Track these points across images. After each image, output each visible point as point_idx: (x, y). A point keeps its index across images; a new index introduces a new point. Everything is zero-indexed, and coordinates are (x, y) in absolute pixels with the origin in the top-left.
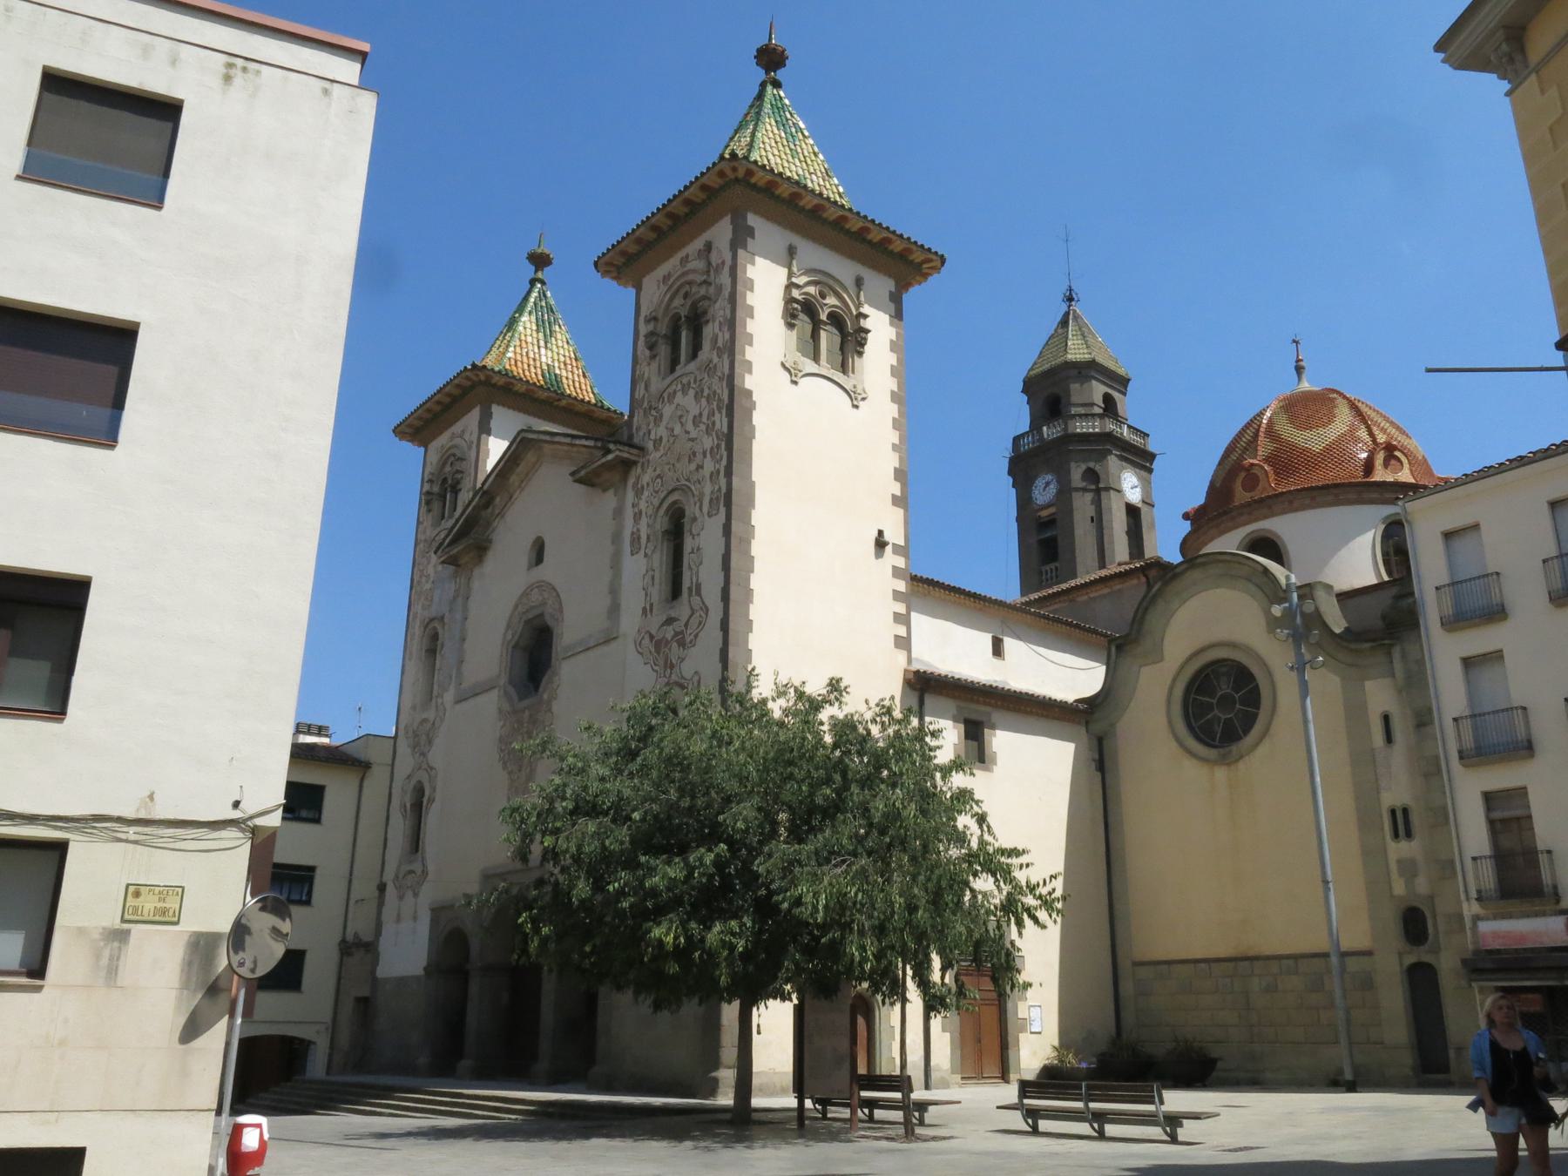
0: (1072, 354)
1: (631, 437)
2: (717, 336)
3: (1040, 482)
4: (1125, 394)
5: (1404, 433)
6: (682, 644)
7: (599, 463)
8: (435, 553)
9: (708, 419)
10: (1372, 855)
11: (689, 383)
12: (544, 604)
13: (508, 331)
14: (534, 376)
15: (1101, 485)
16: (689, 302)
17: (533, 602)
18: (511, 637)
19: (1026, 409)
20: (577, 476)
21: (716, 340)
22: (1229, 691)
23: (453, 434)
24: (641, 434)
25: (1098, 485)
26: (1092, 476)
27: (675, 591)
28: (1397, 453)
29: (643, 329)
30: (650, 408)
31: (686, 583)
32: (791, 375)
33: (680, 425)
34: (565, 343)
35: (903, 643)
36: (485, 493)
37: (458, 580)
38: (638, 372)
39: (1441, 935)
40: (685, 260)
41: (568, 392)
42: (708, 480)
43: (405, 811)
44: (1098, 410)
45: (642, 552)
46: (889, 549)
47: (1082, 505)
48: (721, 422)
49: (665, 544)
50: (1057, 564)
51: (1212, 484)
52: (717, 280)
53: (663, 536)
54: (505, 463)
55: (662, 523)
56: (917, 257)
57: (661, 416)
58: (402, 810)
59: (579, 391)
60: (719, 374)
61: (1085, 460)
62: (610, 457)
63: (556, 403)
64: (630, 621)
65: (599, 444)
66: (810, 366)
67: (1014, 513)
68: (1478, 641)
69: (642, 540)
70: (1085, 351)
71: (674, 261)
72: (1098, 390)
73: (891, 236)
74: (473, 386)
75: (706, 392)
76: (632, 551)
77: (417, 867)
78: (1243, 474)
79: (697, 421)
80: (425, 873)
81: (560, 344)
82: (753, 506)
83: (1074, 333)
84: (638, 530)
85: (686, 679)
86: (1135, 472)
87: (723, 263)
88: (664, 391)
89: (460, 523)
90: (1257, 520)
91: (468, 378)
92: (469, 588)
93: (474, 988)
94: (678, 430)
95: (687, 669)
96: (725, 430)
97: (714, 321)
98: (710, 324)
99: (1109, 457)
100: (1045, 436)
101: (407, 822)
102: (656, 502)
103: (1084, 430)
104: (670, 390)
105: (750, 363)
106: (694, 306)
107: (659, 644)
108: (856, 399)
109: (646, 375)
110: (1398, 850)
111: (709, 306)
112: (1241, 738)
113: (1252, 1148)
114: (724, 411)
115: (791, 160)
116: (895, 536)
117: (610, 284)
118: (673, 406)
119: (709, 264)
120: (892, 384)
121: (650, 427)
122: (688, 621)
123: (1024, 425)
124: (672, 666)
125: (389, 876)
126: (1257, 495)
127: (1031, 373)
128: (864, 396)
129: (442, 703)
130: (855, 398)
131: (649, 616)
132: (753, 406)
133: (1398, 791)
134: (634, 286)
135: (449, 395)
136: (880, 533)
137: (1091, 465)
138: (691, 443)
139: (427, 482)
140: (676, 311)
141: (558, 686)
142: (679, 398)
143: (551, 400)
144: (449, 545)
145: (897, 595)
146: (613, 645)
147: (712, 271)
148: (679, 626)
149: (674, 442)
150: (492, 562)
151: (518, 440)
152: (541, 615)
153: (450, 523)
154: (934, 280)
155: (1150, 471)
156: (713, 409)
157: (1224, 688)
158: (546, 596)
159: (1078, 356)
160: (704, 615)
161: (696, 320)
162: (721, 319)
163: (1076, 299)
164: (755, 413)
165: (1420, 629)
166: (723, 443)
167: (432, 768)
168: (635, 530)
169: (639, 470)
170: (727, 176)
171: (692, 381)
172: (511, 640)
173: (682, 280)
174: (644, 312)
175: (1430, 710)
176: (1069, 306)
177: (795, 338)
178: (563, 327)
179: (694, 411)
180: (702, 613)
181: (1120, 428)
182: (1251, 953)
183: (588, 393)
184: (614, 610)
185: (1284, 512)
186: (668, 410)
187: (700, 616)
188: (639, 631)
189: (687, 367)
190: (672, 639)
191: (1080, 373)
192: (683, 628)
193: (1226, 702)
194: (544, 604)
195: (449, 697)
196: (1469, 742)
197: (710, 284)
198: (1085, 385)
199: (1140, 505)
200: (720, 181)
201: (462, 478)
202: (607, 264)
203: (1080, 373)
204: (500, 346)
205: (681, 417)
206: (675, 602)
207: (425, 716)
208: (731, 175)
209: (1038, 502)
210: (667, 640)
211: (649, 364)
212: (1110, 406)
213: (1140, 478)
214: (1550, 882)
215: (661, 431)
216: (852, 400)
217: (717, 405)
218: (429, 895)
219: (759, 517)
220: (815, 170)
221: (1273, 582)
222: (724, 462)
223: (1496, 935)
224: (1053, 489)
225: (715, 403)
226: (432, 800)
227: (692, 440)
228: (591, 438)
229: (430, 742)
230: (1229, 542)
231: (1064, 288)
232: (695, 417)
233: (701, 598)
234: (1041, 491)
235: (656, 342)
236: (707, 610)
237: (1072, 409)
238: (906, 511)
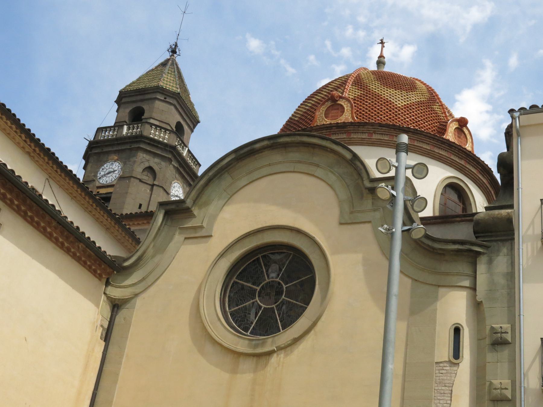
22: (278, 280)
163: (178, 53)
181: (183, 148)
212: (179, 130)
231: (172, 42)
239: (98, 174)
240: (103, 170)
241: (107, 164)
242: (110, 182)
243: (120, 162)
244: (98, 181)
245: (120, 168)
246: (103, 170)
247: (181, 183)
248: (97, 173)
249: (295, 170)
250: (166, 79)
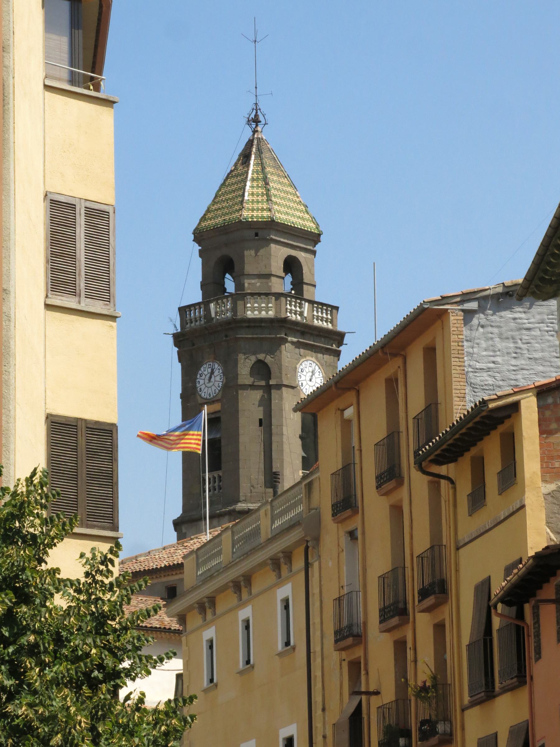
0: (249, 210)
3: (205, 370)
15: (272, 382)
19: (198, 262)
61: (254, 353)
67: (179, 391)
83: (255, 176)
86: (317, 358)
99: (283, 347)
100: (213, 315)
127: (203, 224)
137: (261, 356)
159: (255, 214)
176: (255, 131)
191: (257, 235)
198: (262, 252)
203: (257, 235)
209: (203, 395)
224: (218, 380)
234: (207, 381)
239: (197, 384)
240: (201, 376)
241: (204, 366)
242: (214, 395)
243: (218, 362)
244: (199, 394)
245: (221, 371)
246: (201, 376)
247: (312, 357)
248: (196, 383)
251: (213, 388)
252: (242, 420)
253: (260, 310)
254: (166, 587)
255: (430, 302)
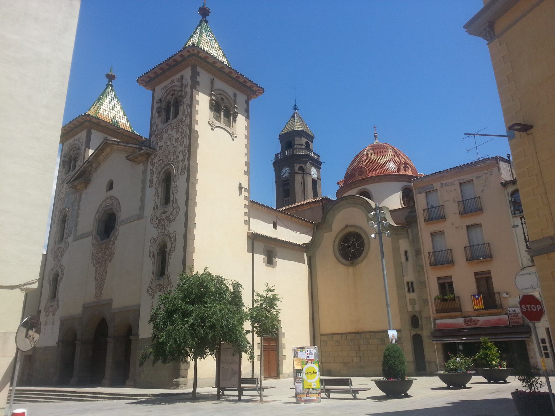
1: (150, 145)
2: (185, 110)
4: (312, 142)
5: (409, 159)
6: (169, 221)
7: (138, 153)
8: (67, 184)
9: (181, 140)
10: (401, 297)
11: (174, 126)
12: (113, 204)
13: (98, 102)
14: (108, 120)
16: (174, 97)
17: (108, 204)
18: (98, 217)
20: (128, 158)
21: (185, 112)
23: (75, 139)
24: (154, 144)
25: (304, 173)
26: (301, 169)
27: (167, 201)
28: (408, 166)
29: (156, 106)
30: (158, 134)
31: (171, 199)
32: (211, 127)
33: (170, 141)
34: (120, 109)
35: (247, 223)
36: (89, 162)
37: (76, 195)
38: (153, 121)
39: (423, 325)
40: (172, 82)
41: (121, 127)
42: (181, 162)
43: (50, 282)
44: (303, 147)
45: (154, 187)
46: (243, 189)
47: (298, 178)
48: (186, 142)
49: (163, 184)
50: (289, 198)
51: (347, 173)
52: (185, 90)
53: (162, 182)
54: (98, 151)
55: (162, 176)
56: (255, 89)
57: (162, 138)
58: (49, 282)
59: (125, 127)
60: (186, 124)
61: (299, 164)
62: (142, 151)
63: (117, 131)
64: (149, 211)
65: (138, 146)
66: (218, 124)
68: (436, 227)
69: (154, 182)
70: (300, 127)
71: (169, 81)
72: (304, 140)
73: (247, 80)
74: (84, 122)
75: (180, 130)
76: (150, 186)
77: (55, 304)
78: (358, 170)
79: (176, 140)
80: (58, 306)
81: (118, 109)
82: (197, 172)
84: (152, 179)
85: (170, 233)
87: (188, 84)
88: (164, 129)
89: (78, 173)
90: (363, 185)
91: (82, 119)
92: (80, 197)
93: (78, 349)
94: (169, 143)
95: (171, 230)
96: (188, 144)
97: (184, 105)
98: (182, 106)
100: (287, 154)
101: (51, 287)
102: (160, 169)
103: (299, 153)
104: (166, 129)
105: (197, 121)
106: (176, 99)
107: (160, 221)
108: (233, 137)
109: (157, 122)
110: (410, 296)
111: (182, 99)
112: (357, 258)
113: (214, 404)
114: (187, 137)
115: (211, 49)
116: (245, 185)
117: (142, 88)
118: (167, 135)
119: (182, 84)
120: (245, 132)
121: (158, 142)
122: (172, 212)
123: (279, 151)
124: (165, 229)
125: (42, 307)
126: (363, 177)
128: (236, 135)
129: (68, 241)
130: (233, 136)
131: (156, 210)
132: (198, 136)
133: (410, 276)
134: (151, 90)
135: (74, 124)
136: (240, 184)
138: (174, 148)
139: (63, 157)
140: (169, 100)
141: (118, 235)
142: (170, 131)
143: (115, 130)
144: (73, 181)
145: (245, 206)
146: (141, 221)
147: (183, 86)
148: (168, 214)
149: (167, 148)
150: (91, 188)
151: (104, 143)
152: (111, 209)
153: (73, 173)
154: (260, 97)
155: (320, 168)
156: (183, 136)
157: (352, 241)
158: (113, 201)
160: (178, 211)
161: (177, 104)
162: (187, 104)
163: (297, 109)
164: (199, 139)
165: (417, 223)
166: (187, 149)
167: (62, 266)
168: (151, 179)
169: (153, 157)
170: (190, 52)
171: (175, 126)
172: (98, 218)
173: (171, 89)
174: (156, 99)
175: (420, 249)
177: (213, 114)
178: (119, 103)
179: (175, 136)
180: (177, 210)
182: (361, 331)
183: (128, 128)
184: (142, 207)
185: (372, 183)
186: (165, 136)
187: (177, 211)
188: (152, 216)
189: (173, 120)
190: (165, 219)
191: (298, 134)
192: (170, 215)
193: (353, 245)
194: (113, 204)
195: (71, 239)
196: (433, 261)
197: (183, 91)
199: (317, 179)
200: (188, 54)
201: (78, 156)
202: (142, 80)
204: (94, 108)
205: (170, 139)
206: (166, 206)
207: (60, 246)
208: (192, 52)
210: (163, 219)
211: (158, 119)
212: (308, 146)
213: (317, 170)
214: (500, 304)
215: (162, 143)
216: (232, 137)
217: (185, 135)
218: (60, 313)
219: (199, 176)
220: (220, 54)
221: (369, 206)
222: (187, 156)
223: (442, 324)
224: (288, 173)
225: (184, 134)
226: (62, 278)
227: (175, 147)
228: (134, 144)
229: (62, 256)
230: (353, 192)
231: (294, 105)
232: (176, 139)
233: (177, 204)
235: (161, 110)
236: (179, 208)
237: (296, 146)
238: (249, 177)
249: (354, 335)
250: (296, 125)
251: (287, 174)
252: (296, 183)
253: (301, 152)
254: (274, 267)
255: (350, 166)
